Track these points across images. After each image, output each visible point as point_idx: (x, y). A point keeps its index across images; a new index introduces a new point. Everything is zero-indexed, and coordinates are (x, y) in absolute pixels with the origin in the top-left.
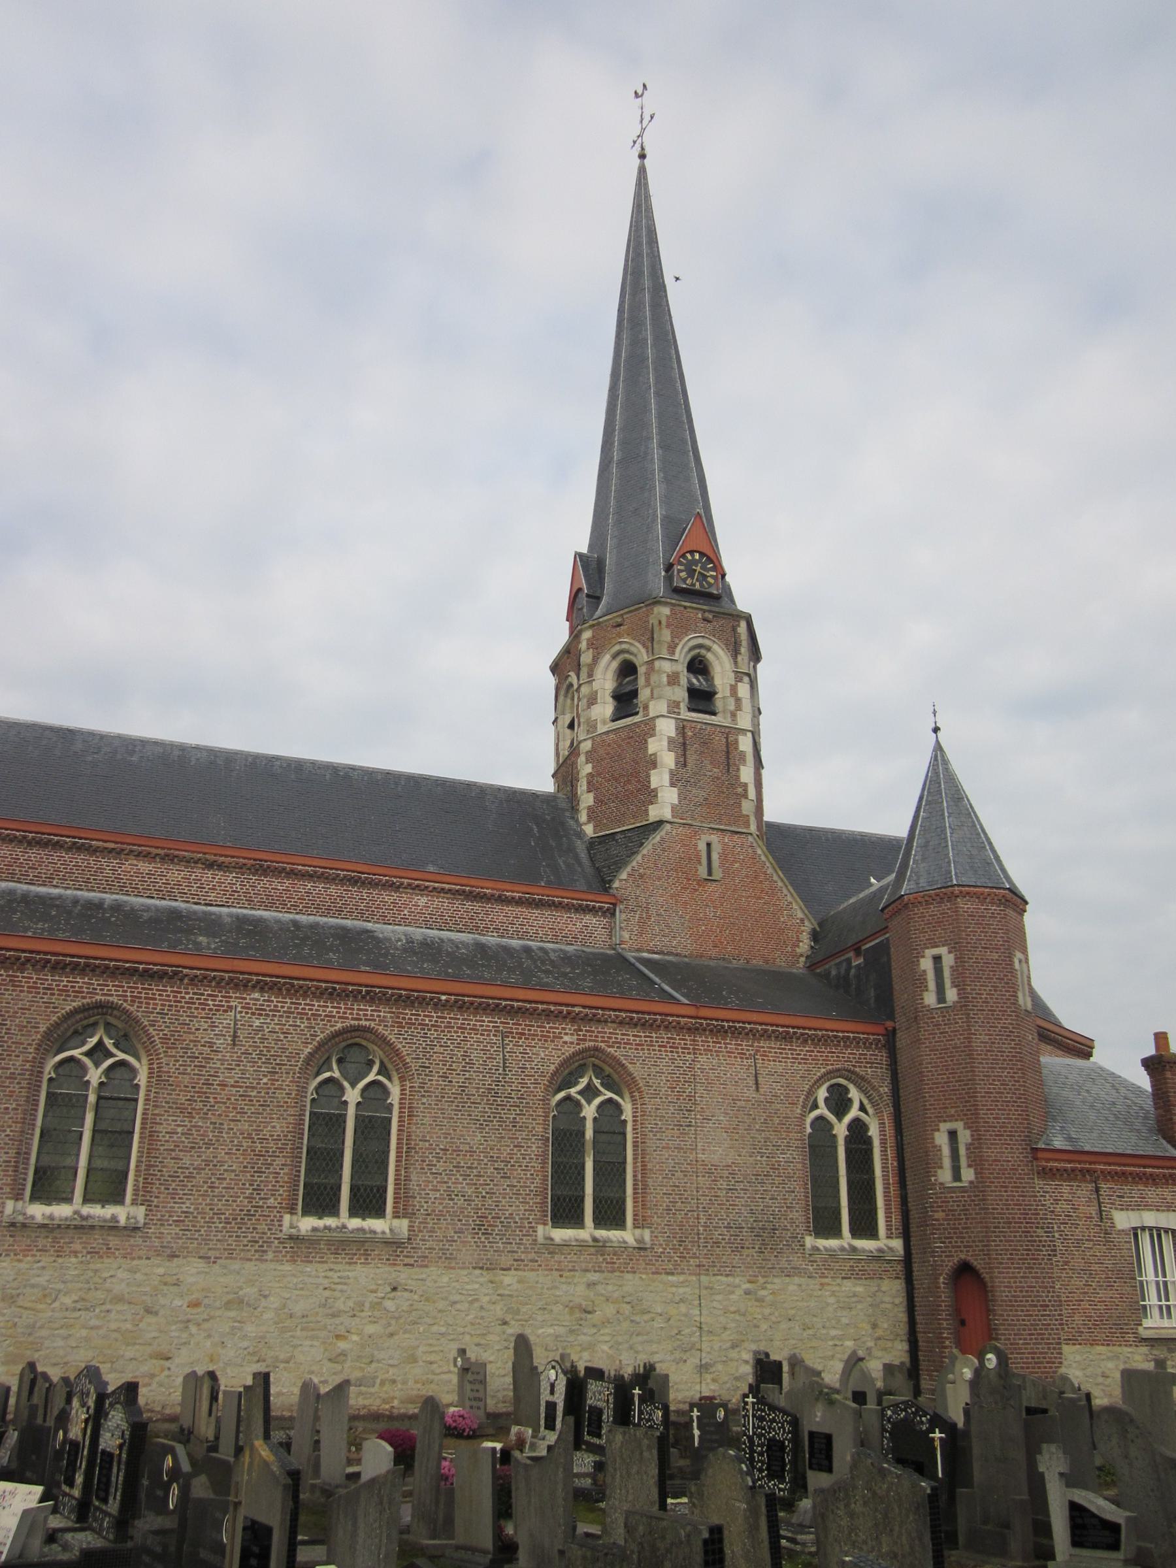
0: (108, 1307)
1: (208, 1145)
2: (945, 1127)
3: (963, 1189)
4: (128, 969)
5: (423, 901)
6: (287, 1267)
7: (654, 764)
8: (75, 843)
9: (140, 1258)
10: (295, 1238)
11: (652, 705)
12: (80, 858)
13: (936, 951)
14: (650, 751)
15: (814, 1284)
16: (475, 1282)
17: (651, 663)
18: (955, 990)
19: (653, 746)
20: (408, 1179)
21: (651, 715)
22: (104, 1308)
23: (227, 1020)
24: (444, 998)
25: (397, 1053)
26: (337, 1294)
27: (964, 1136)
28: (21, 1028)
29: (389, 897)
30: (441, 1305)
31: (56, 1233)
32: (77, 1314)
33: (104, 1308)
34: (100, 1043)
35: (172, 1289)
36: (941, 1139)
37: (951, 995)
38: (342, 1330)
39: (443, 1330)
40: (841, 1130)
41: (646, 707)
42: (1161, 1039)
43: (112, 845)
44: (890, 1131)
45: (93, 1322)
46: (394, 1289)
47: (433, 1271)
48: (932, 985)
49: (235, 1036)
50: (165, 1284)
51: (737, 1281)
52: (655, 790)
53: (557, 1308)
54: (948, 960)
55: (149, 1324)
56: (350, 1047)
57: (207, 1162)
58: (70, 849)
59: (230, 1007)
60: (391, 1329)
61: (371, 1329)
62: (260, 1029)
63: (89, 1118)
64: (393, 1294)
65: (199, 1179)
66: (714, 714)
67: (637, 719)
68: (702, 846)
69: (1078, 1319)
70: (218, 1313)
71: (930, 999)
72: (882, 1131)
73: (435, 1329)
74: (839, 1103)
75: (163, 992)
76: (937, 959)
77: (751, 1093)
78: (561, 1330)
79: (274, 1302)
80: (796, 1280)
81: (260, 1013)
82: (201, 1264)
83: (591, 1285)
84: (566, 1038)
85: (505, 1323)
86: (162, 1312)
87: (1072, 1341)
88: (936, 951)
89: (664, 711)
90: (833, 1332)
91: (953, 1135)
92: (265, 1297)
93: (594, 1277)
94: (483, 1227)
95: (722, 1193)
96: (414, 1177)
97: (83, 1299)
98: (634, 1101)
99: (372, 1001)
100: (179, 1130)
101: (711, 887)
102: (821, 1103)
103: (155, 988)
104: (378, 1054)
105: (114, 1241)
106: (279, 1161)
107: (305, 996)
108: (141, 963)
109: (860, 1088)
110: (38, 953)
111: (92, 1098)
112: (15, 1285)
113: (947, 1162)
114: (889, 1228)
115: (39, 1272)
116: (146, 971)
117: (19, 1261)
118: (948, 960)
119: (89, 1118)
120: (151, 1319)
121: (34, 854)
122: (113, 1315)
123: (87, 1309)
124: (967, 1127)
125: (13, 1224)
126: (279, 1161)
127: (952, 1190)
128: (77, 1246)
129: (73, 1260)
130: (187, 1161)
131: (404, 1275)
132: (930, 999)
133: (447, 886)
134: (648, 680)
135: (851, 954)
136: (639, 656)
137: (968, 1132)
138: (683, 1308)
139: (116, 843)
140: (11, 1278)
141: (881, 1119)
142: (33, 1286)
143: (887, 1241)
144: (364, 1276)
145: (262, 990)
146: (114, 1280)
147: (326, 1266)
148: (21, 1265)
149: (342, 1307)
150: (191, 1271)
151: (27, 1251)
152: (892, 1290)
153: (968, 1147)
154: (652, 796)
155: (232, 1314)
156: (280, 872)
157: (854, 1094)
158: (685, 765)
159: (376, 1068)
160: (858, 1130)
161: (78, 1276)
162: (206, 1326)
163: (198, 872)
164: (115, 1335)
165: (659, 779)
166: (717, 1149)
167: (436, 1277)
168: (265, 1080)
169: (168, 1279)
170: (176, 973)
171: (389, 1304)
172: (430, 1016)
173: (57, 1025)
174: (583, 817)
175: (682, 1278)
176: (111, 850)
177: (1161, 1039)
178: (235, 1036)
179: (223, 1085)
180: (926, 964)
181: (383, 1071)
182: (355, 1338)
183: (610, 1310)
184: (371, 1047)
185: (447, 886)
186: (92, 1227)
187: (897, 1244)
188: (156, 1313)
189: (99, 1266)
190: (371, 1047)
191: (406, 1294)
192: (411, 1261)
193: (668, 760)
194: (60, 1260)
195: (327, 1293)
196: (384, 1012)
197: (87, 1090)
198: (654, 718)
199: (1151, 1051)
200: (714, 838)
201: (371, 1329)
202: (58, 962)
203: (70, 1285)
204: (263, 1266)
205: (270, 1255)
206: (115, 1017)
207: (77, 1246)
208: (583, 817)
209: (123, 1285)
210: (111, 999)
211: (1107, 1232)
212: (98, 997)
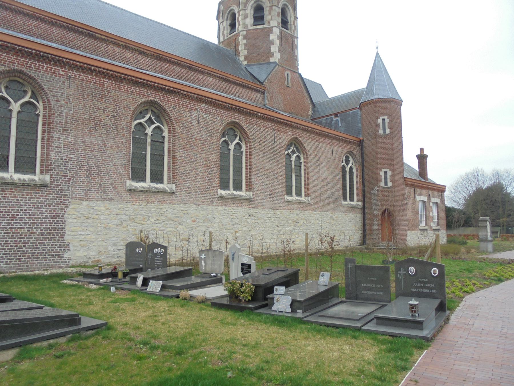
0: (166, 222)
1: (193, 162)
2: (383, 170)
3: (388, 188)
4: (161, 88)
5: (211, 79)
6: (220, 208)
7: (272, 43)
8: (89, 33)
9: (175, 204)
10: (222, 198)
11: (271, 22)
12: (91, 41)
13: (383, 117)
14: (271, 39)
15: (344, 214)
16: (270, 213)
17: (271, 7)
18: (389, 130)
19: (272, 37)
20: (251, 178)
21: (271, 26)
22: (165, 223)
23: (195, 113)
24: (259, 114)
25: (246, 133)
26: (235, 217)
27: (389, 173)
28: (124, 108)
29: (201, 76)
30: (262, 221)
31: (146, 194)
32: (156, 225)
33: (165, 223)
34: (150, 116)
35: (187, 215)
36: (382, 174)
37: (388, 131)
38: (237, 229)
39: (263, 229)
40: (348, 169)
41: (269, 23)
42: (422, 150)
43: (104, 37)
44: (360, 171)
45: (162, 228)
46: (250, 216)
47: (260, 209)
48: (381, 127)
49: (198, 120)
50: (184, 214)
51: (329, 213)
52: (273, 53)
53: (290, 222)
54: (387, 121)
55: (180, 228)
56: (233, 129)
57: (194, 169)
58: (86, 36)
59: (196, 109)
60: (250, 229)
61: (244, 229)
62: (206, 119)
63: (149, 148)
64: (249, 217)
65: (191, 175)
66: (288, 30)
67: (265, 26)
68: (286, 75)
69: (410, 224)
70: (201, 224)
71: (381, 132)
72: (357, 171)
73: (261, 228)
74: (347, 162)
75: (174, 99)
76: (384, 120)
77: (331, 156)
78: (291, 228)
79: (217, 220)
80: (341, 213)
81: (205, 112)
82: (194, 207)
83: (298, 214)
84: (290, 133)
85: (278, 226)
86: (184, 224)
87: (409, 230)
88: (383, 117)
89: (276, 25)
90: (348, 228)
91: (386, 172)
92: (215, 218)
93: (298, 212)
94: (272, 196)
95: (325, 187)
96: (253, 177)
97: (158, 220)
98: (304, 156)
99: (239, 113)
100: (184, 155)
101: (288, 89)
102: (344, 161)
103: (171, 97)
104: (238, 133)
105: (166, 197)
106: (215, 169)
107: (219, 108)
108: (166, 86)
109: (353, 158)
110: (128, 75)
111: (149, 140)
112: (133, 214)
113: (383, 180)
114: (357, 199)
115: (141, 209)
116: (168, 89)
117: (134, 205)
118: (387, 121)
119: (149, 148)
120: (180, 227)
121: (71, 35)
122: (168, 225)
123: (159, 223)
124: (390, 170)
125: (130, 190)
126: (215, 169)
127: (384, 188)
128: (154, 199)
129: (153, 205)
130: (187, 168)
131: (252, 211)
132: (381, 132)
133: (219, 75)
134: (270, 14)
135: (333, 116)
136: (266, 4)
137: (391, 172)
138: (318, 221)
139: (106, 36)
140: (131, 212)
141: (357, 167)
142: (140, 215)
143: (357, 203)
144: (242, 211)
145: (206, 103)
146: (167, 212)
147: (231, 208)
148: (135, 206)
149: (236, 222)
150: (192, 209)
151: (136, 201)
152: (359, 216)
153: (390, 176)
154: (272, 55)
155: (206, 224)
156: (165, 60)
157: (351, 159)
158: (282, 45)
159: (238, 138)
160: (351, 168)
161: (155, 211)
162: (198, 229)
163: (136, 55)
164: (170, 233)
165: (274, 49)
166: (325, 174)
167: (260, 212)
168: (209, 139)
169: (186, 212)
170: (178, 92)
171: (248, 220)
172: (255, 121)
173: (136, 108)
174: (242, 58)
175: (317, 212)
176: (103, 39)
177: (422, 150)
178: (198, 120)
179: (196, 139)
180: (380, 121)
181: (240, 139)
182: (240, 232)
183: (302, 222)
184: (236, 130)
185: (219, 75)
186: (158, 192)
187: (360, 203)
188: (182, 225)
189: (162, 207)
190: (236, 130)
191: (253, 217)
192: (254, 206)
193: (278, 42)
194: (148, 204)
195: (232, 217)
196: (242, 117)
197: (147, 137)
198: (272, 27)
199: (419, 153)
200: (289, 73)
201: (244, 229)
202: (136, 81)
203: (153, 214)
204: (213, 207)
205: (215, 204)
206: (155, 108)
207: (154, 199)
208: (242, 58)
209: (170, 215)
210: (156, 100)
211: (415, 201)
212: (151, 98)
